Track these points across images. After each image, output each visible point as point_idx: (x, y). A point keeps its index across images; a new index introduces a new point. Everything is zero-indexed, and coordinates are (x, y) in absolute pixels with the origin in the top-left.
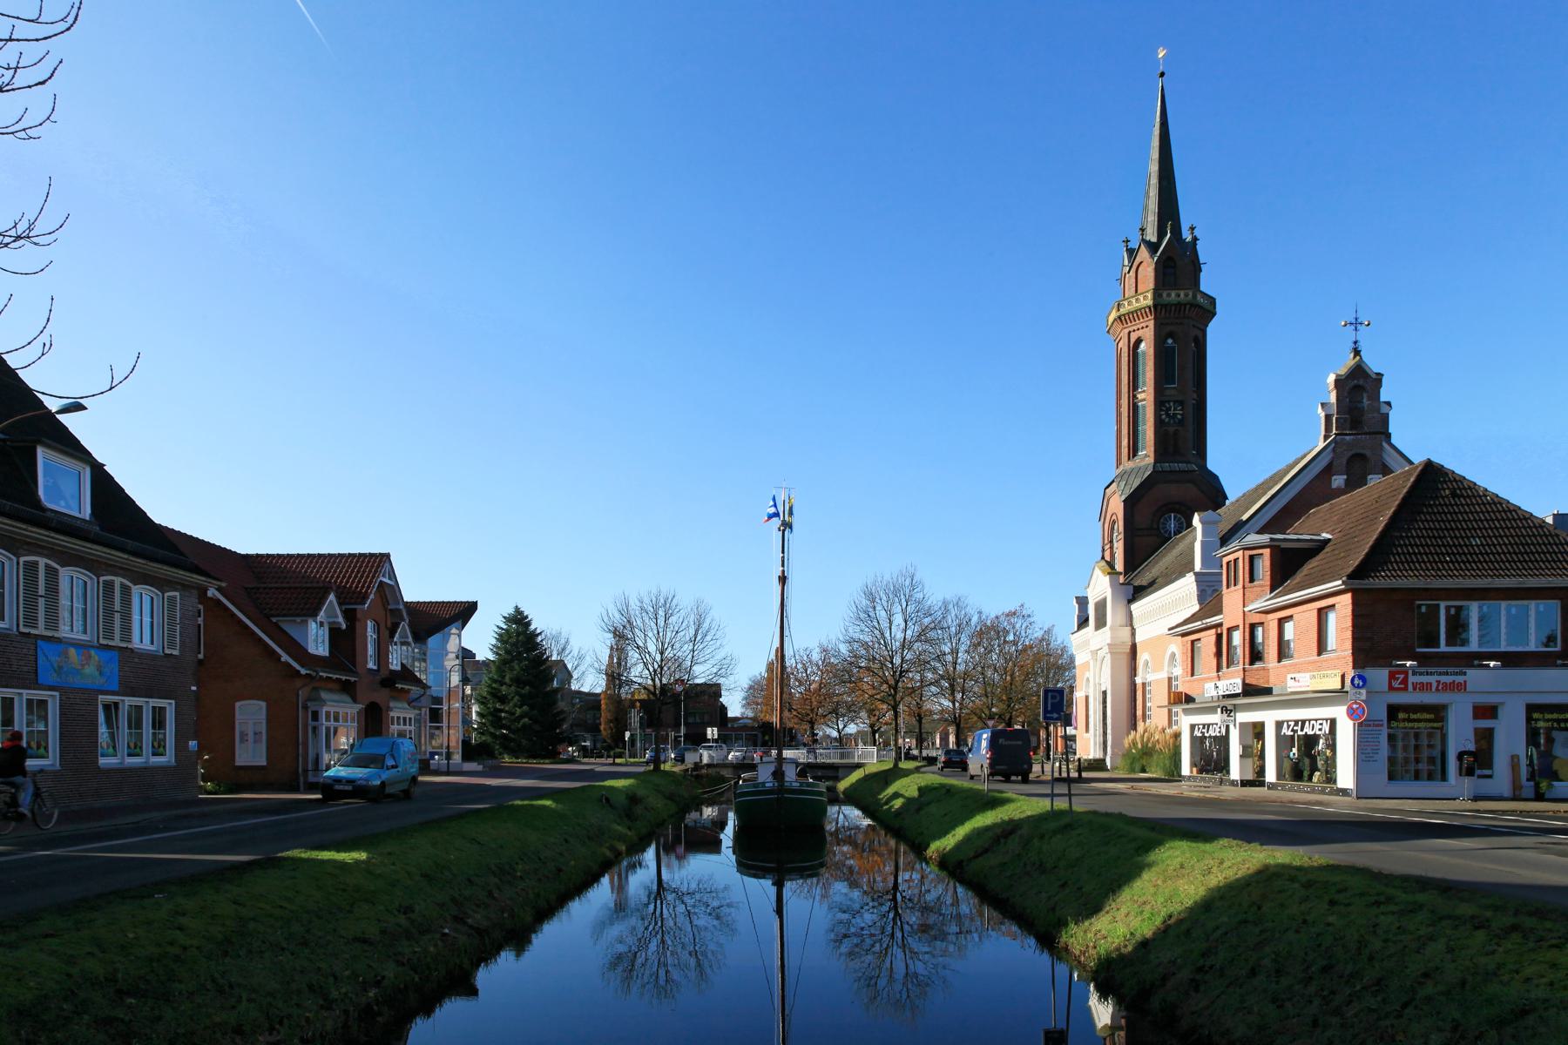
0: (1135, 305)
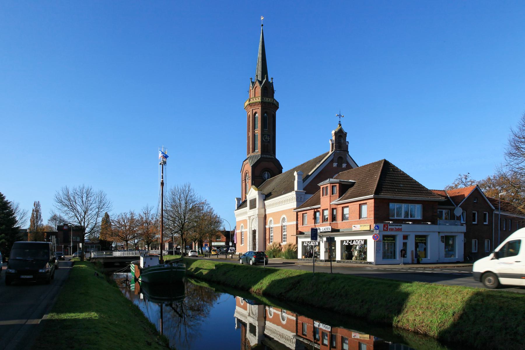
0: (255, 101)
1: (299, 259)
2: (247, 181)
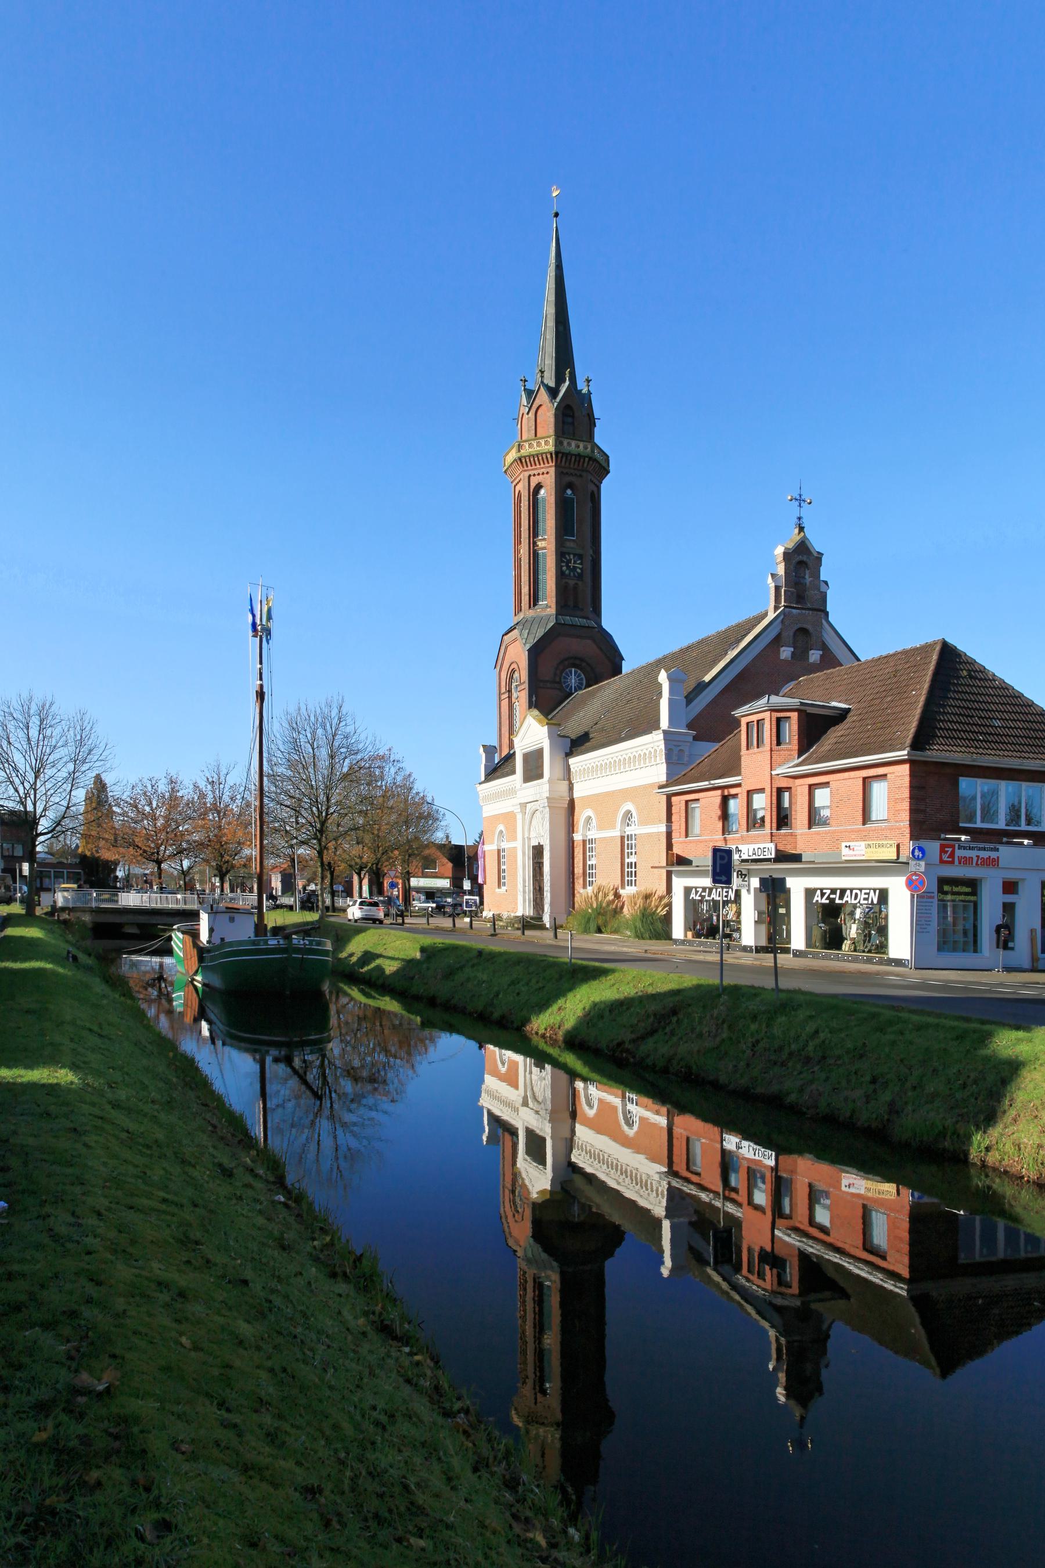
0: (536, 449)
1: (676, 941)
2: (515, 695)
